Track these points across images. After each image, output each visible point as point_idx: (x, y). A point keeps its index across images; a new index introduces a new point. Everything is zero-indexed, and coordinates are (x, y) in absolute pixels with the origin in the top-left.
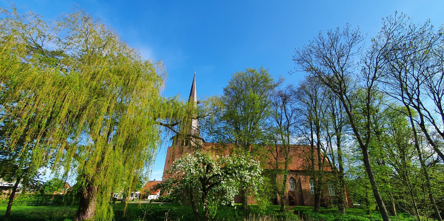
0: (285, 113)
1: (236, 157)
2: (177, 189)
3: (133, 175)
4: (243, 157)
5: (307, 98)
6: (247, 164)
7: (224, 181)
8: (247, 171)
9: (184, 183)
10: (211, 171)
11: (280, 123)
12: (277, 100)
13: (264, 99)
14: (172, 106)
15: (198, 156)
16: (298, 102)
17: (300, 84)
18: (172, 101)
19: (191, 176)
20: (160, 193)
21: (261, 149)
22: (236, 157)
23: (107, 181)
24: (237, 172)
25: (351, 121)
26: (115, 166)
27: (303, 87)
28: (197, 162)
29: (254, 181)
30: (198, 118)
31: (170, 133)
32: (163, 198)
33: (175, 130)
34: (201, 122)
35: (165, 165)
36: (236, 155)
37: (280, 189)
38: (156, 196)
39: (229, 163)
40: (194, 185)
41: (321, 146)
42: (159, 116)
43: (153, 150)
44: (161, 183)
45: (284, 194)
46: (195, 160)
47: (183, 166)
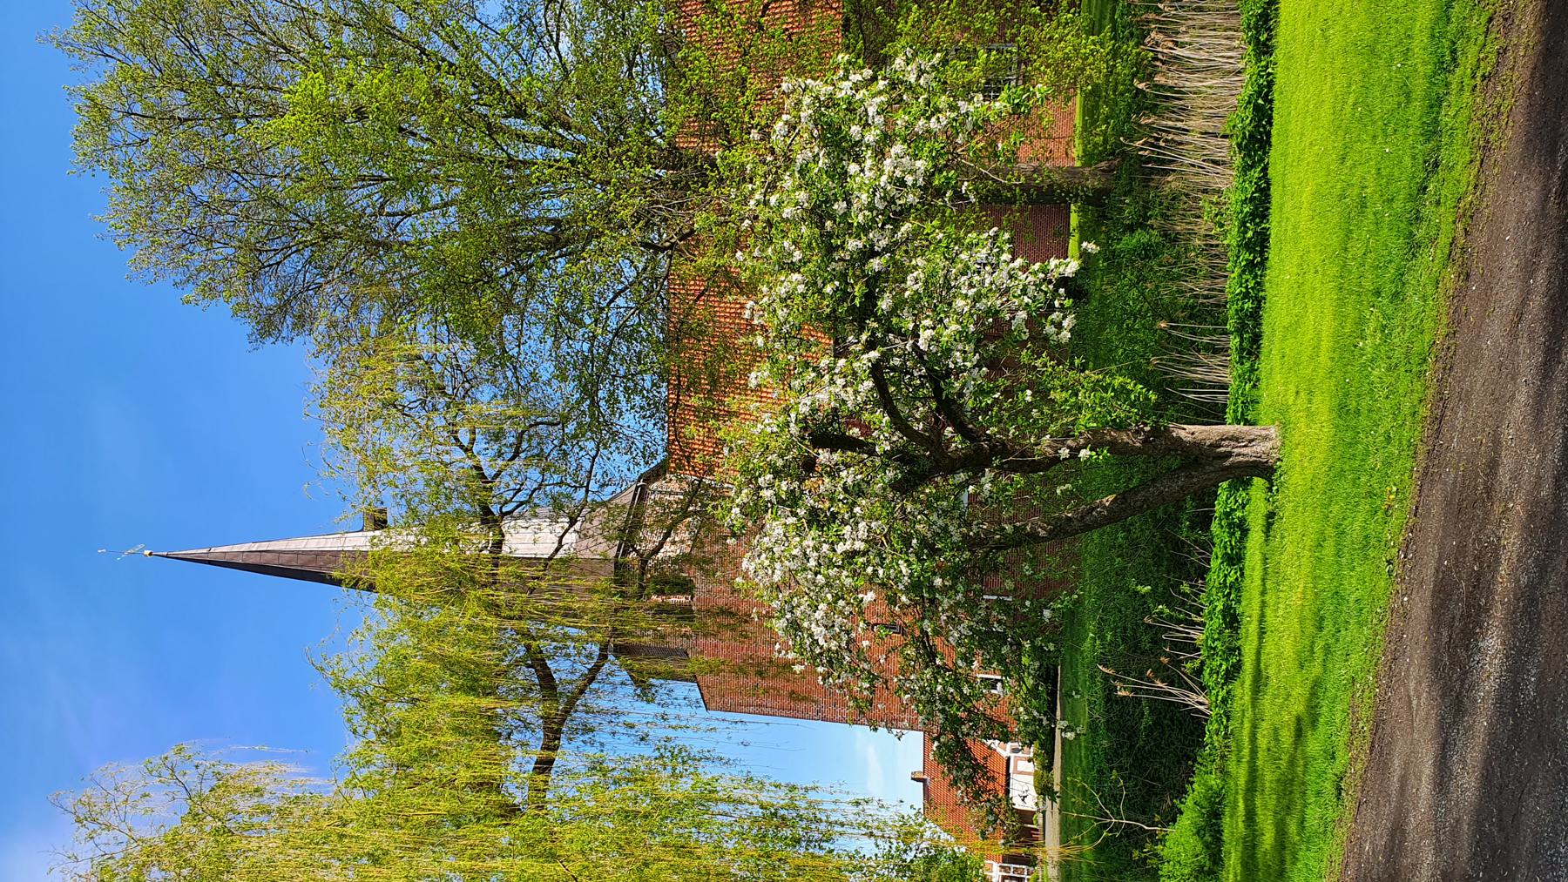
2: (972, 637)
8: (853, 168)
9: (932, 588)
10: (853, 418)
13: (322, 29)
14: (414, 701)
15: (755, 512)
18: (371, 706)
21: (699, 63)
32: (1026, 724)
38: (1017, 759)
40: (945, 529)
43: (723, 807)
44: (937, 738)
47: (822, 606)
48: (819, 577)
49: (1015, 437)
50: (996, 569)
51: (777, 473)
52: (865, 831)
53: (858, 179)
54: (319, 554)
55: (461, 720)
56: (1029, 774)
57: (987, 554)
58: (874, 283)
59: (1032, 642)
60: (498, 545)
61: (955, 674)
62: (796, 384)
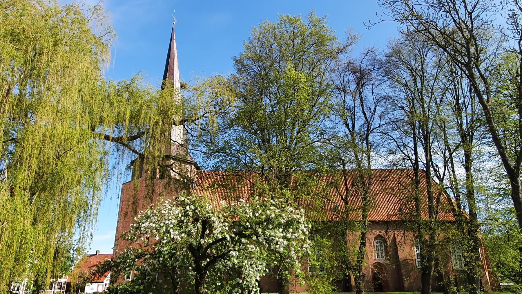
0: (362, 105)
1: (258, 202)
2: (144, 270)
3: (53, 244)
4: (273, 203)
5: (406, 76)
6: (280, 216)
7: (235, 252)
8: (281, 230)
9: (159, 257)
10: (211, 232)
11: (350, 128)
12: (345, 81)
13: (319, 79)
14: (128, 100)
15: (183, 204)
16: (388, 83)
17: (389, 45)
18: (127, 88)
19: (171, 243)
20: (109, 278)
21: (313, 183)
22: (258, 202)
23: (2, 260)
24: (260, 233)
25: (489, 121)
26: (16, 230)
27: (397, 52)
28: (182, 216)
29: (293, 249)
30: (182, 122)
31: (126, 155)
32: (116, 288)
33: (137, 149)
34: (189, 131)
35: (118, 222)
36: (259, 199)
37: (353, 259)
38: (103, 285)
39: (245, 215)
40: (178, 261)
41: (435, 170)
42: (102, 121)
43: (91, 193)
44: (112, 260)
45: (360, 269)
46: (177, 213)
47: (154, 225)
48: (163, 224)
49: (206, 281)
50: (165, 277)
51: (194, 210)
52: (82, 237)
53: (277, 232)
54: (173, 70)
55: (122, 114)
56: (97, 290)
57: (170, 274)
58: (249, 237)
59: (142, 289)
60: (175, 124)
61: (133, 265)
62: (221, 215)
